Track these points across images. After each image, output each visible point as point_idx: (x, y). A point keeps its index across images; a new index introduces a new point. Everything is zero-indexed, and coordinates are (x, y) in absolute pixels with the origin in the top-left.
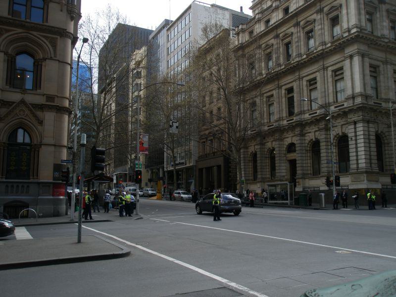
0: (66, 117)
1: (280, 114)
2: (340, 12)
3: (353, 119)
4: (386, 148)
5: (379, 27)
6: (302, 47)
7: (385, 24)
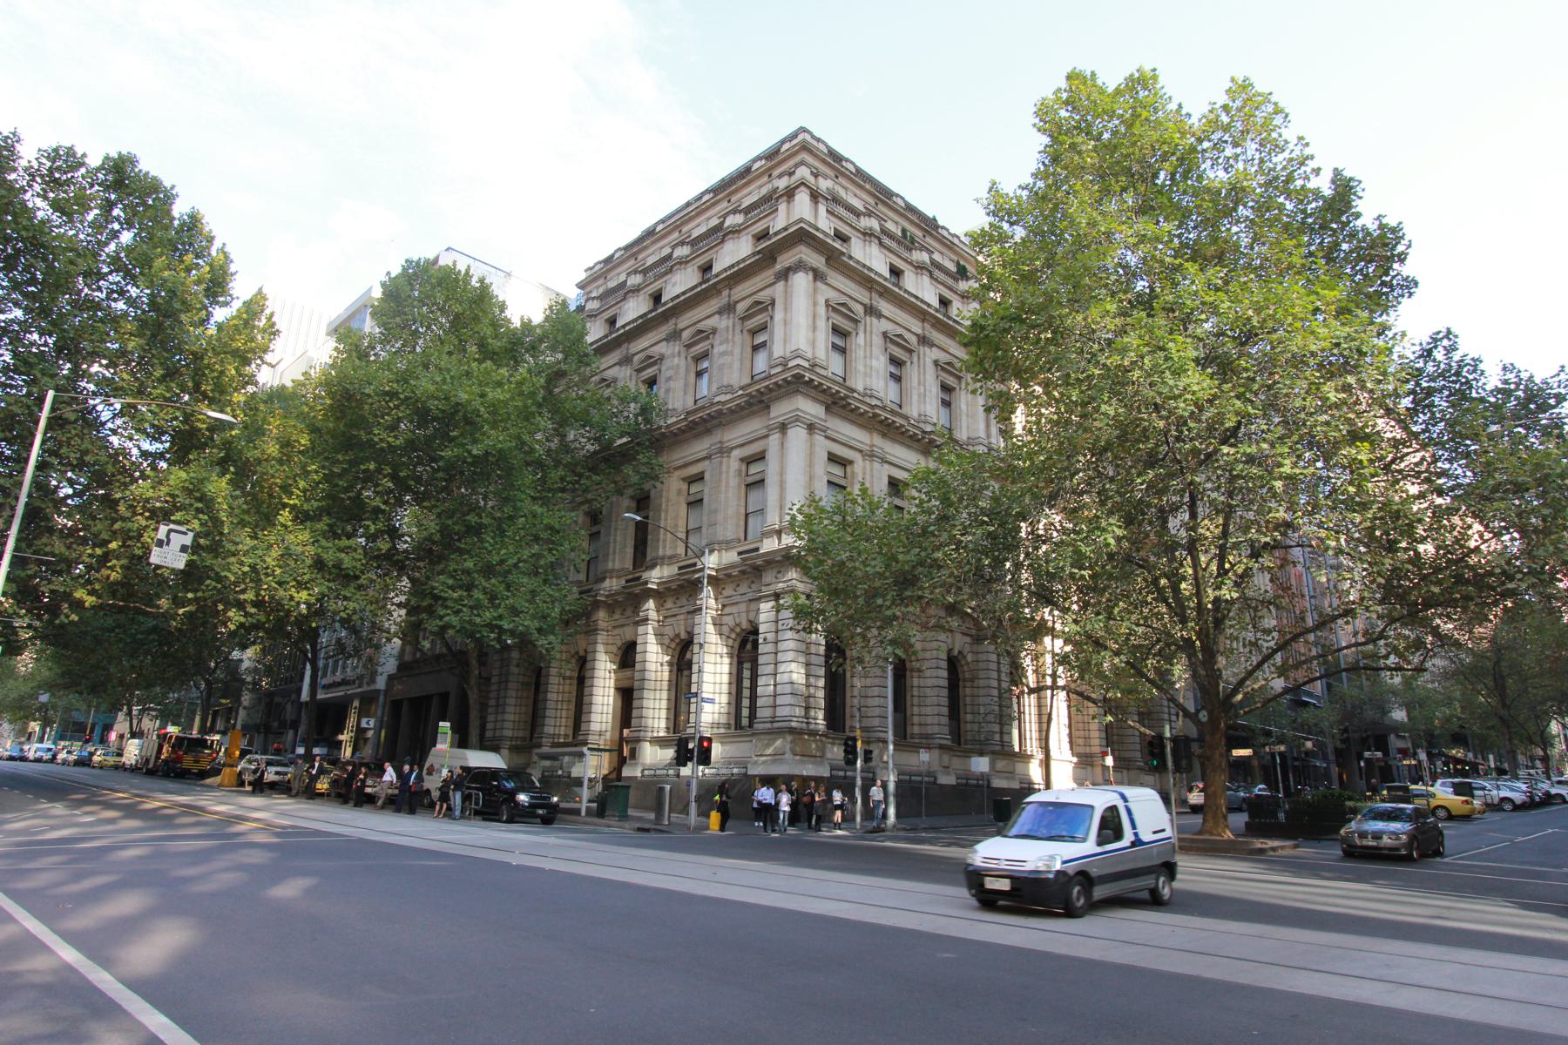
0: (1032, 685)
3: (772, 587)
4: (915, 681)
5: (861, 368)
7: (874, 363)
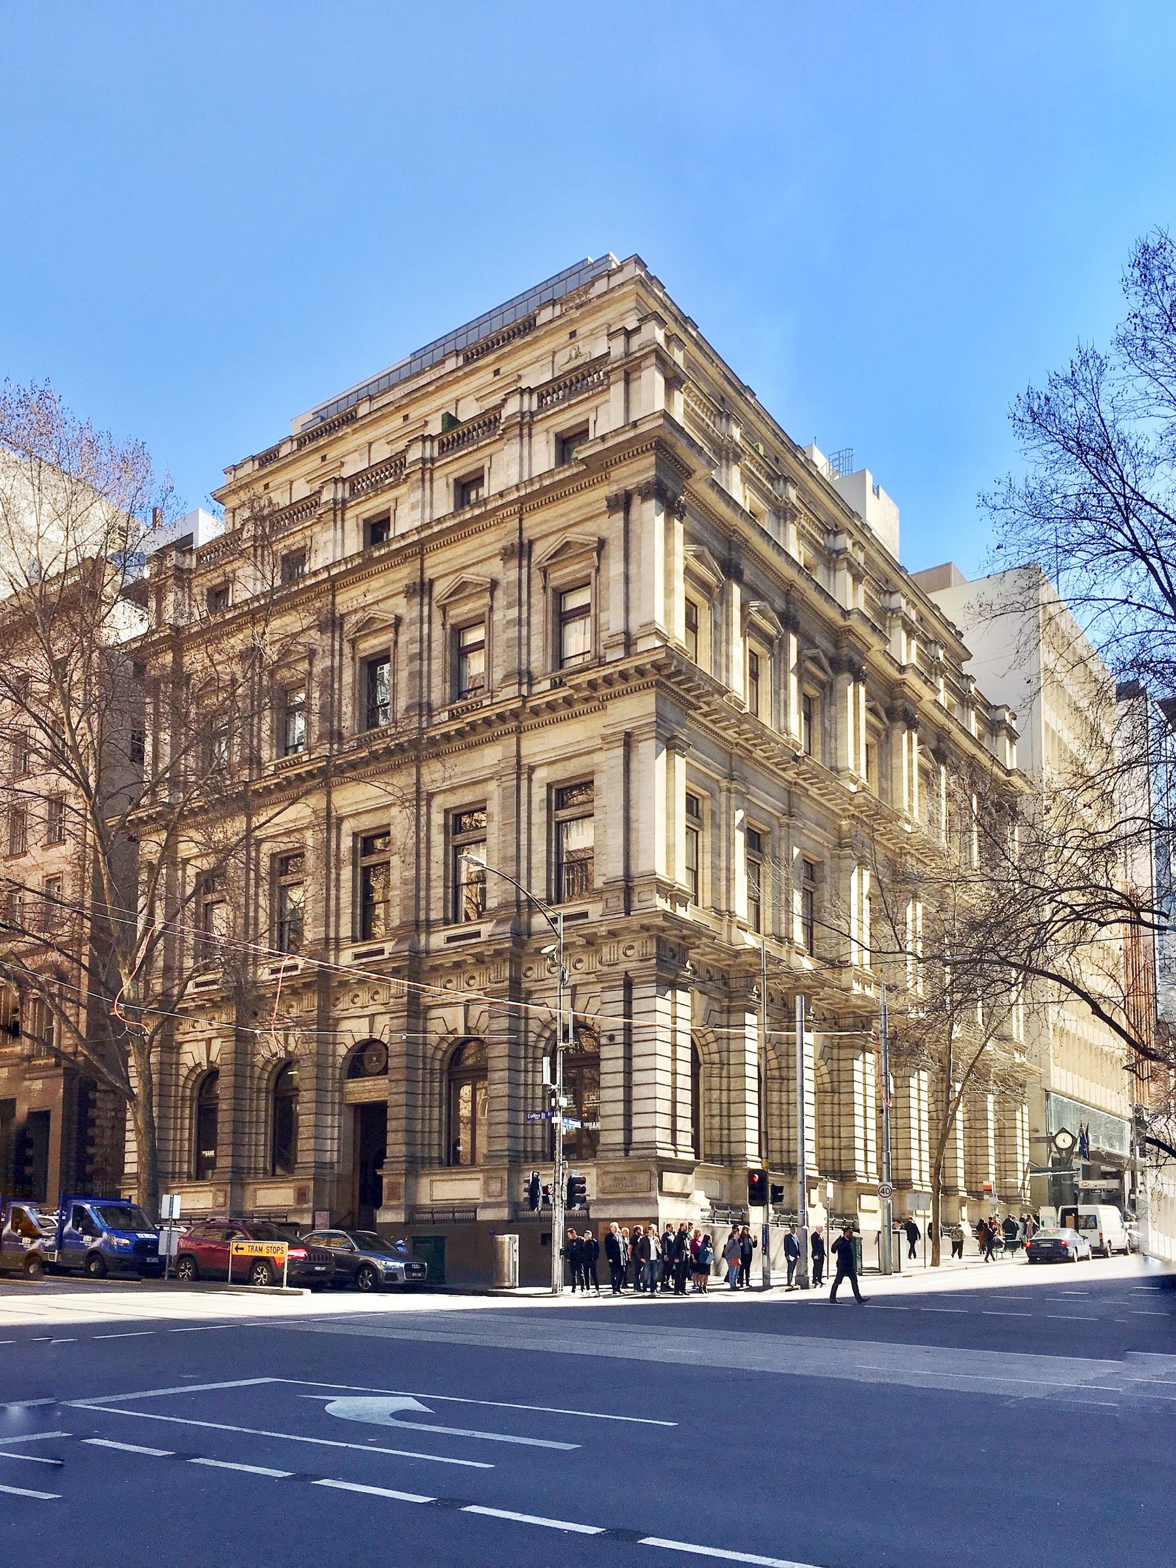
1: (327, 925)
2: (598, 570)
6: (437, 680)
